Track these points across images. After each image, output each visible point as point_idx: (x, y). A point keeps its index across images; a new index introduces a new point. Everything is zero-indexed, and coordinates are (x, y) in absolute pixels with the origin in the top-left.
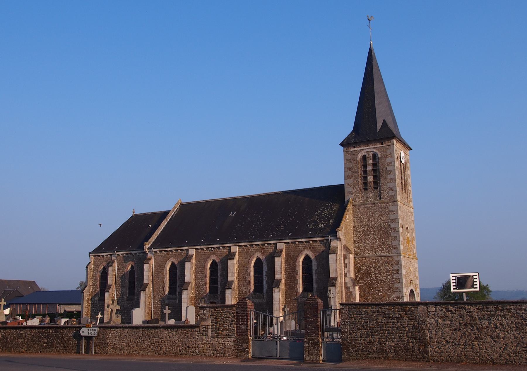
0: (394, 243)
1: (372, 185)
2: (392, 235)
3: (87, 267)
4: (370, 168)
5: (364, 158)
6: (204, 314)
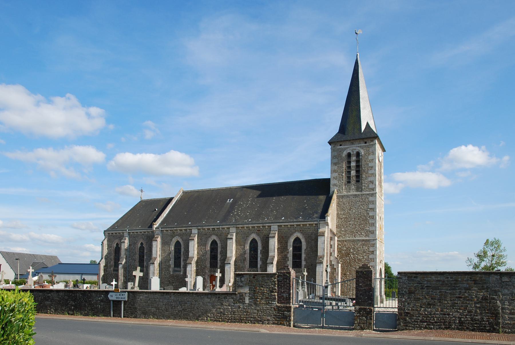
0: (371, 229)
1: (354, 179)
2: (370, 222)
3: (102, 243)
4: (353, 164)
5: (349, 155)
6: (242, 282)
